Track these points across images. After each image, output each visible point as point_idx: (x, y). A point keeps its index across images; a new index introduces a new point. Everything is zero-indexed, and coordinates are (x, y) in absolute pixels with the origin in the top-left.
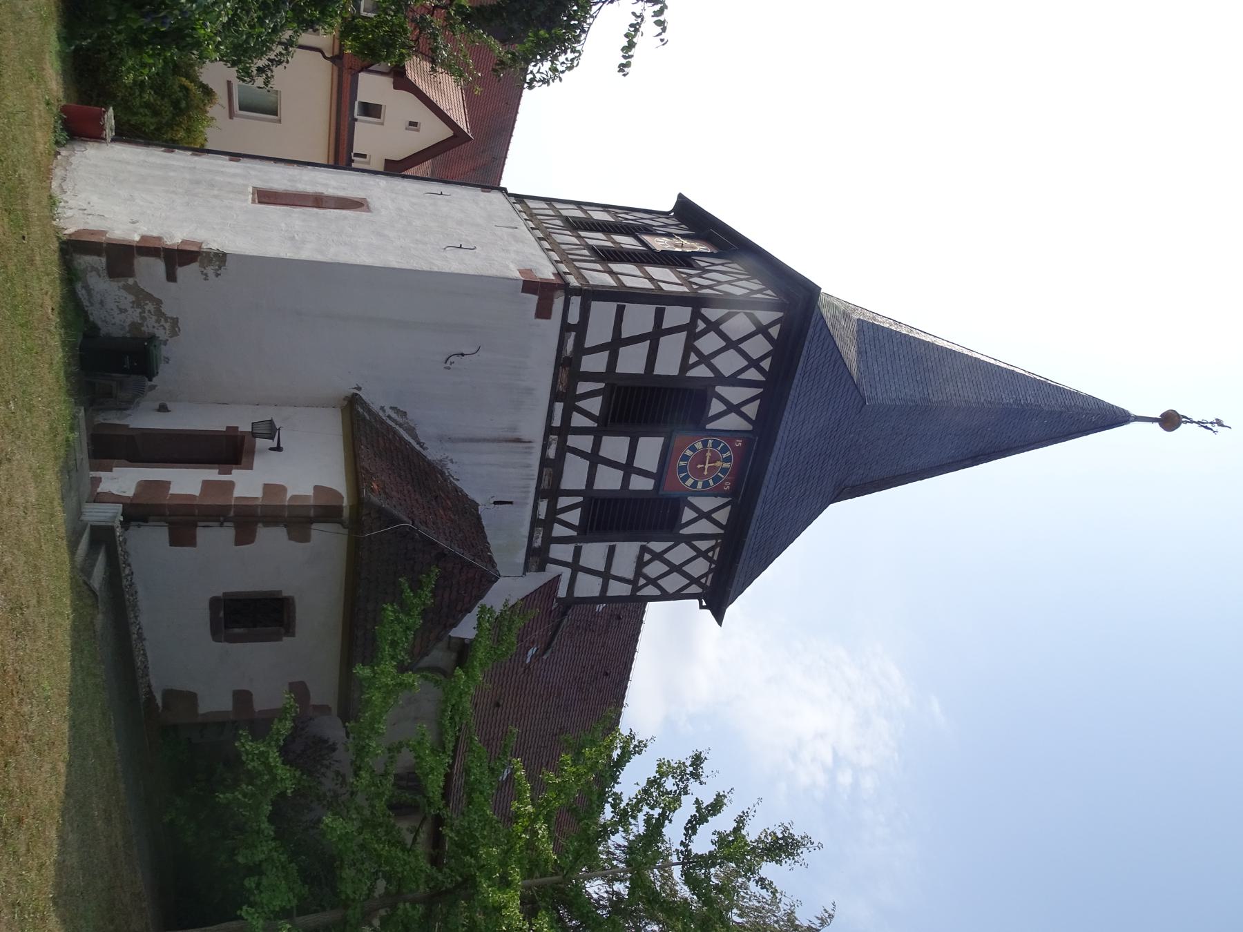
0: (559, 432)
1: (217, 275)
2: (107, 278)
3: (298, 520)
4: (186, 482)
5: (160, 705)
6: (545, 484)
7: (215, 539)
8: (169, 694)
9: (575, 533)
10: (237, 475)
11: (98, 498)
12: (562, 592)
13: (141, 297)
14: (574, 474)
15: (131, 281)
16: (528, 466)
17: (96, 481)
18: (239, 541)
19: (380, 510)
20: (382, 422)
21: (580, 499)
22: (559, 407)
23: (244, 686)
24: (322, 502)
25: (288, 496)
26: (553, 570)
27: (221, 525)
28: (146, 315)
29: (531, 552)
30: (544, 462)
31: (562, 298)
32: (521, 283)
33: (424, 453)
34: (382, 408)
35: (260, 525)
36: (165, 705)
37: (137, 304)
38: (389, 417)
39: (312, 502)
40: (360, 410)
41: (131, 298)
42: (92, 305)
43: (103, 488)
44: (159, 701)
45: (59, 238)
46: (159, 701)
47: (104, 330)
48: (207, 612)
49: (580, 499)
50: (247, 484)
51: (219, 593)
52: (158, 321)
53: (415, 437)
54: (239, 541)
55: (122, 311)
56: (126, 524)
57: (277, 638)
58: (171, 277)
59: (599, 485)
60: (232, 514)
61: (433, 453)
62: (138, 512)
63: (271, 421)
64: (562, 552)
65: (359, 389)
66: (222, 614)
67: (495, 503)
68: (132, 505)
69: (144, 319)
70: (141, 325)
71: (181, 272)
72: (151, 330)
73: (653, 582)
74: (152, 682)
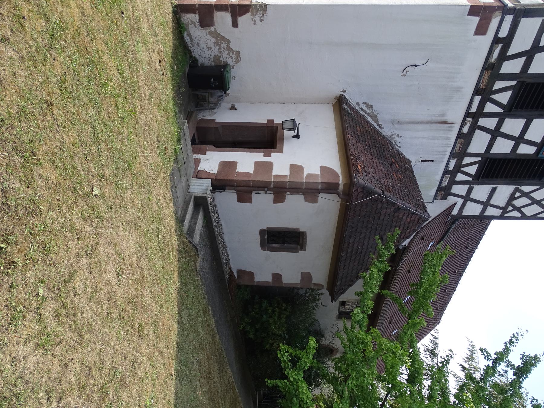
0: (473, 117)
1: (262, 20)
2: (200, 28)
3: (311, 191)
4: (246, 162)
5: (236, 276)
6: (457, 150)
7: (262, 200)
8: (240, 272)
9: (470, 179)
10: (275, 158)
11: (199, 175)
12: (455, 212)
13: (219, 38)
14: (479, 143)
15: (213, 29)
16: (448, 139)
17: (197, 162)
18: (275, 201)
19: (364, 187)
20: (357, 113)
21: (480, 159)
22: (478, 99)
23: (278, 272)
24: (326, 180)
25: (305, 174)
26: (451, 200)
27: (266, 193)
28: (222, 50)
29: (440, 189)
30: (460, 135)
31: (499, 18)
32: (469, 7)
33: (381, 131)
34: (358, 104)
35: (288, 193)
36: (238, 276)
37: (217, 43)
38: (362, 109)
39: (320, 180)
40: (345, 106)
41: (214, 40)
42: (193, 46)
43: (201, 167)
44: (235, 274)
45: (172, 4)
46: (235, 274)
47: (200, 62)
48: (259, 236)
49: (480, 159)
50: (280, 164)
51: (265, 227)
52: (229, 54)
53: (376, 121)
54: (275, 201)
55: (209, 48)
56: (213, 191)
57: (295, 250)
58: (235, 24)
59: (495, 150)
60: (272, 186)
61: (386, 131)
62: (219, 184)
63: (294, 120)
64: (461, 190)
65: (345, 91)
66: (266, 237)
67: (422, 161)
68: (216, 180)
69: (221, 53)
70: (220, 57)
71: (241, 20)
72: (225, 60)
73: (519, 209)
74: (232, 266)
